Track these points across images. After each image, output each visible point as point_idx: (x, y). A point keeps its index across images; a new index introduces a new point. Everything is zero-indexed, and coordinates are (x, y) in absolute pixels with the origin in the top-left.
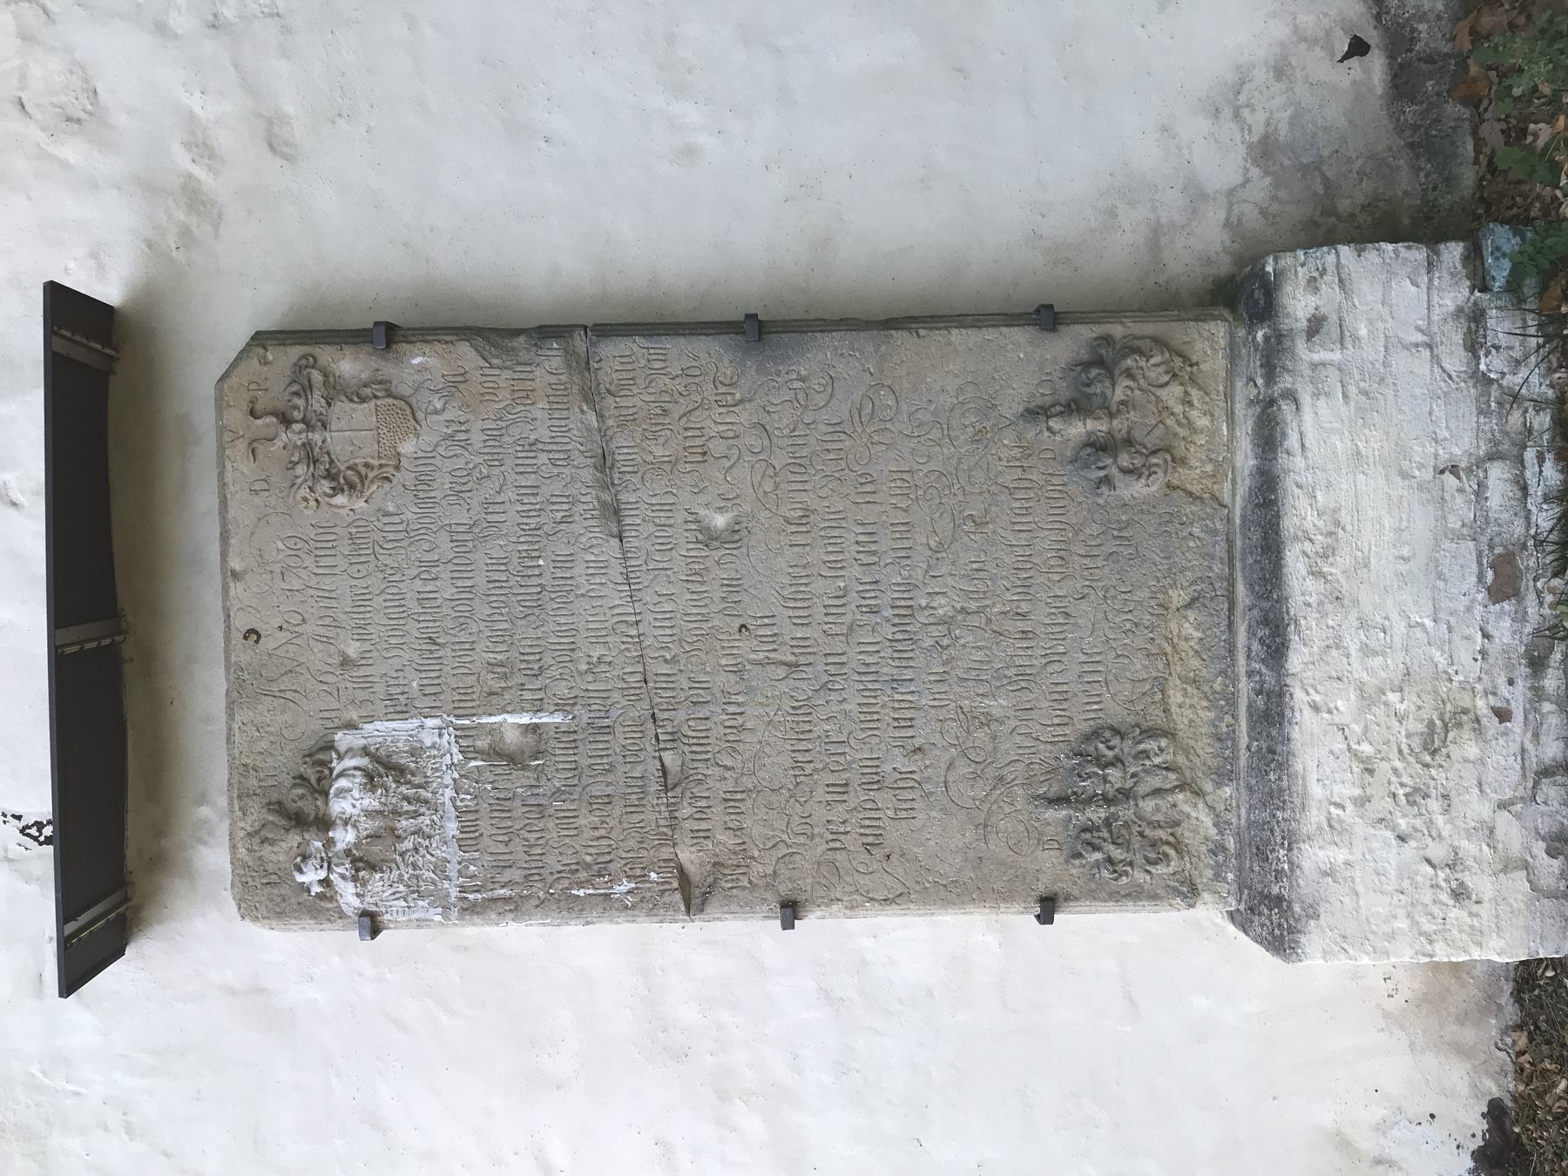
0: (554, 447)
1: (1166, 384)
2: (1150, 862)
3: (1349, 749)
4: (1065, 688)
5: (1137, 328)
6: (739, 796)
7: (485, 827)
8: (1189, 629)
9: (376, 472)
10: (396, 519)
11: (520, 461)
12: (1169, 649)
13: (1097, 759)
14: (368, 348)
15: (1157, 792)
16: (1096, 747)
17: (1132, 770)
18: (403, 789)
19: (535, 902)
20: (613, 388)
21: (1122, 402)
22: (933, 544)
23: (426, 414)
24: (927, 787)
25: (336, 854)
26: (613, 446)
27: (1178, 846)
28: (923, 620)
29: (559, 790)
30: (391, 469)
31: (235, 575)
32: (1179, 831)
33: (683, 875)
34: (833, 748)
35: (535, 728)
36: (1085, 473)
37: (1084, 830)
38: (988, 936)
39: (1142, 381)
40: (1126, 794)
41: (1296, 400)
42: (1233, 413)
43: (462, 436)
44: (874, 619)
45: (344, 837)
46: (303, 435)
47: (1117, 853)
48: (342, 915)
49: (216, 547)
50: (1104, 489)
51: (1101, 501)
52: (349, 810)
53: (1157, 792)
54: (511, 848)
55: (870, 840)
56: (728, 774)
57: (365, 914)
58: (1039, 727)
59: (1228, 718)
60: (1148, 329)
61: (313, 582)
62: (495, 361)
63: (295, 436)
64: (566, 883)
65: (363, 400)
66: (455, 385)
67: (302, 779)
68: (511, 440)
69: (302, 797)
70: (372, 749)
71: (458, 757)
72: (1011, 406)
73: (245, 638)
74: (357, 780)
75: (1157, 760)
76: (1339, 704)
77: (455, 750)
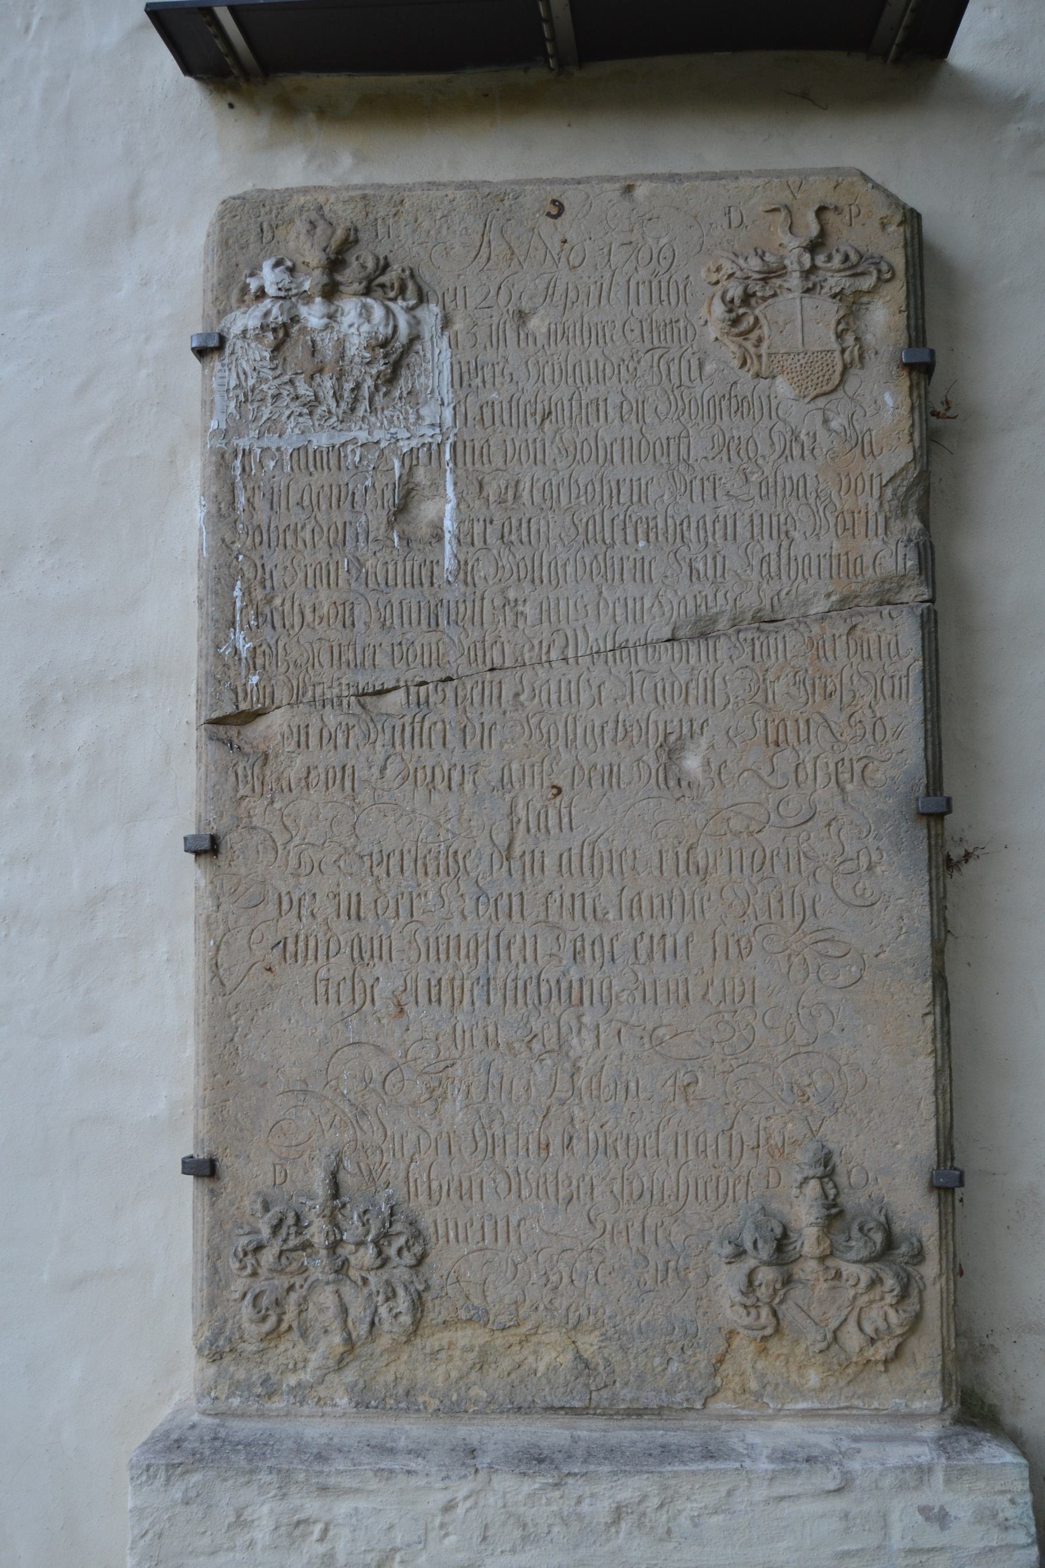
0: (784, 561)
1: (861, 1329)
2: (256, 1298)
3: (395, 1550)
4: (476, 1196)
5: (933, 1296)
6: (348, 784)
7: (321, 478)
8: (548, 1356)
9: (752, 350)
10: (695, 374)
11: (766, 519)
12: (523, 1330)
13: (386, 1235)
14: (903, 339)
15: (344, 1310)
16: (401, 1237)
17: (372, 1278)
18: (369, 382)
19: (228, 539)
20: (858, 632)
21: (838, 1275)
22: (661, 1032)
23: (824, 410)
24: (354, 1020)
25: (294, 306)
26: (786, 631)
27: (275, 1334)
28: (565, 1018)
29: (362, 565)
30: (756, 368)
31: (629, 189)
32: (295, 1335)
33: (254, 715)
34: (404, 903)
35: (439, 537)
36: (749, 1224)
37: (298, 1218)
38: (164, 1092)
39: (865, 1298)
40: (342, 1269)
41: (838, 1491)
42: (825, 1416)
43: (796, 452)
44: (567, 955)
45: (313, 315)
46: (796, 266)
47: (268, 1257)
48: (221, 314)
49: (661, 169)
50: (728, 1249)
51: (712, 1246)
52: (346, 320)
53: (344, 1310)
54: (295, 509)
55: (291, 947)
56: (375, 771)
57: (222, 339)
58: (427, 1162)
59: (434, 1404)
60: (933, 1310)
61: (620, 279)
62: (889, 492)
63: (795, 257)
64: (249, 574)
65: (839, 336)
66: (859, 443)
67: (384, 267)
68: (792, 509)
69: (363, 267)
70: (418, 347)
71: (405, 446)
72: (836, 1134)
73: (554, 202)
74: (381, 329)
75: (383, 1311)
76: (452, 1539)
77: (414, 443)
